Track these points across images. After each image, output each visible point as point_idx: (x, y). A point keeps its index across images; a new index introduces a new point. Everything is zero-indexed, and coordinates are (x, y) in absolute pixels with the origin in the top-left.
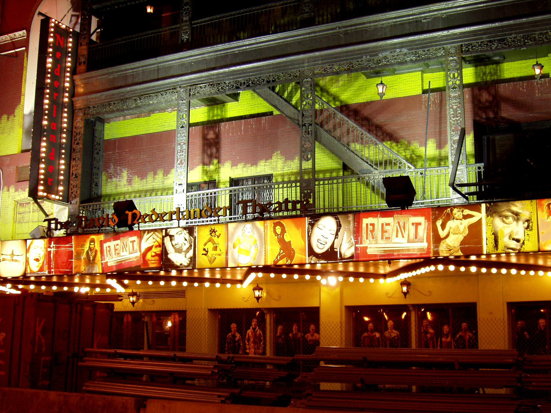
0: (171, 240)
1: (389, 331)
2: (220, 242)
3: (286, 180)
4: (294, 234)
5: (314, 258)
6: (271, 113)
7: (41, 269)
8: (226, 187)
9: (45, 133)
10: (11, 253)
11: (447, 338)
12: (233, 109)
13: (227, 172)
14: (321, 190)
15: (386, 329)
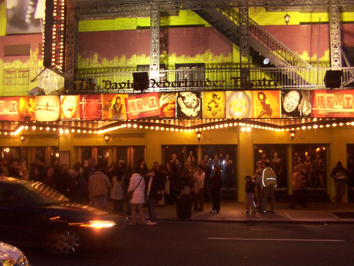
0: (183, 100)
1: (275, 158)
2: (221, 103)
3: (214, 67)
4: (272, 100)
5: (285, 115)
6: (204, 26)
7: (74, 116)
8: (173, 69)
9: (55, 22)
10: (46, 104)
11: (308, 162)
12: (174, 21)
13: (173, 60)
14: (257, 74)
15: (273, 157)
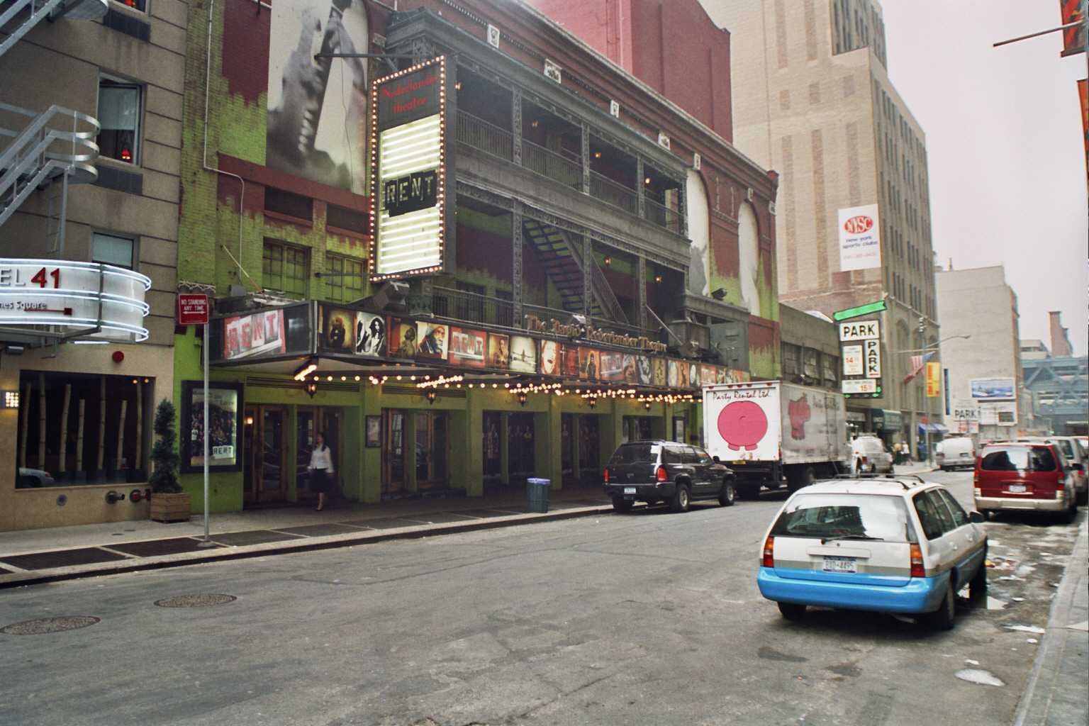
10: (521, 353)
